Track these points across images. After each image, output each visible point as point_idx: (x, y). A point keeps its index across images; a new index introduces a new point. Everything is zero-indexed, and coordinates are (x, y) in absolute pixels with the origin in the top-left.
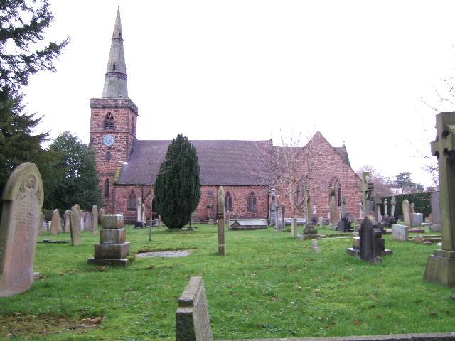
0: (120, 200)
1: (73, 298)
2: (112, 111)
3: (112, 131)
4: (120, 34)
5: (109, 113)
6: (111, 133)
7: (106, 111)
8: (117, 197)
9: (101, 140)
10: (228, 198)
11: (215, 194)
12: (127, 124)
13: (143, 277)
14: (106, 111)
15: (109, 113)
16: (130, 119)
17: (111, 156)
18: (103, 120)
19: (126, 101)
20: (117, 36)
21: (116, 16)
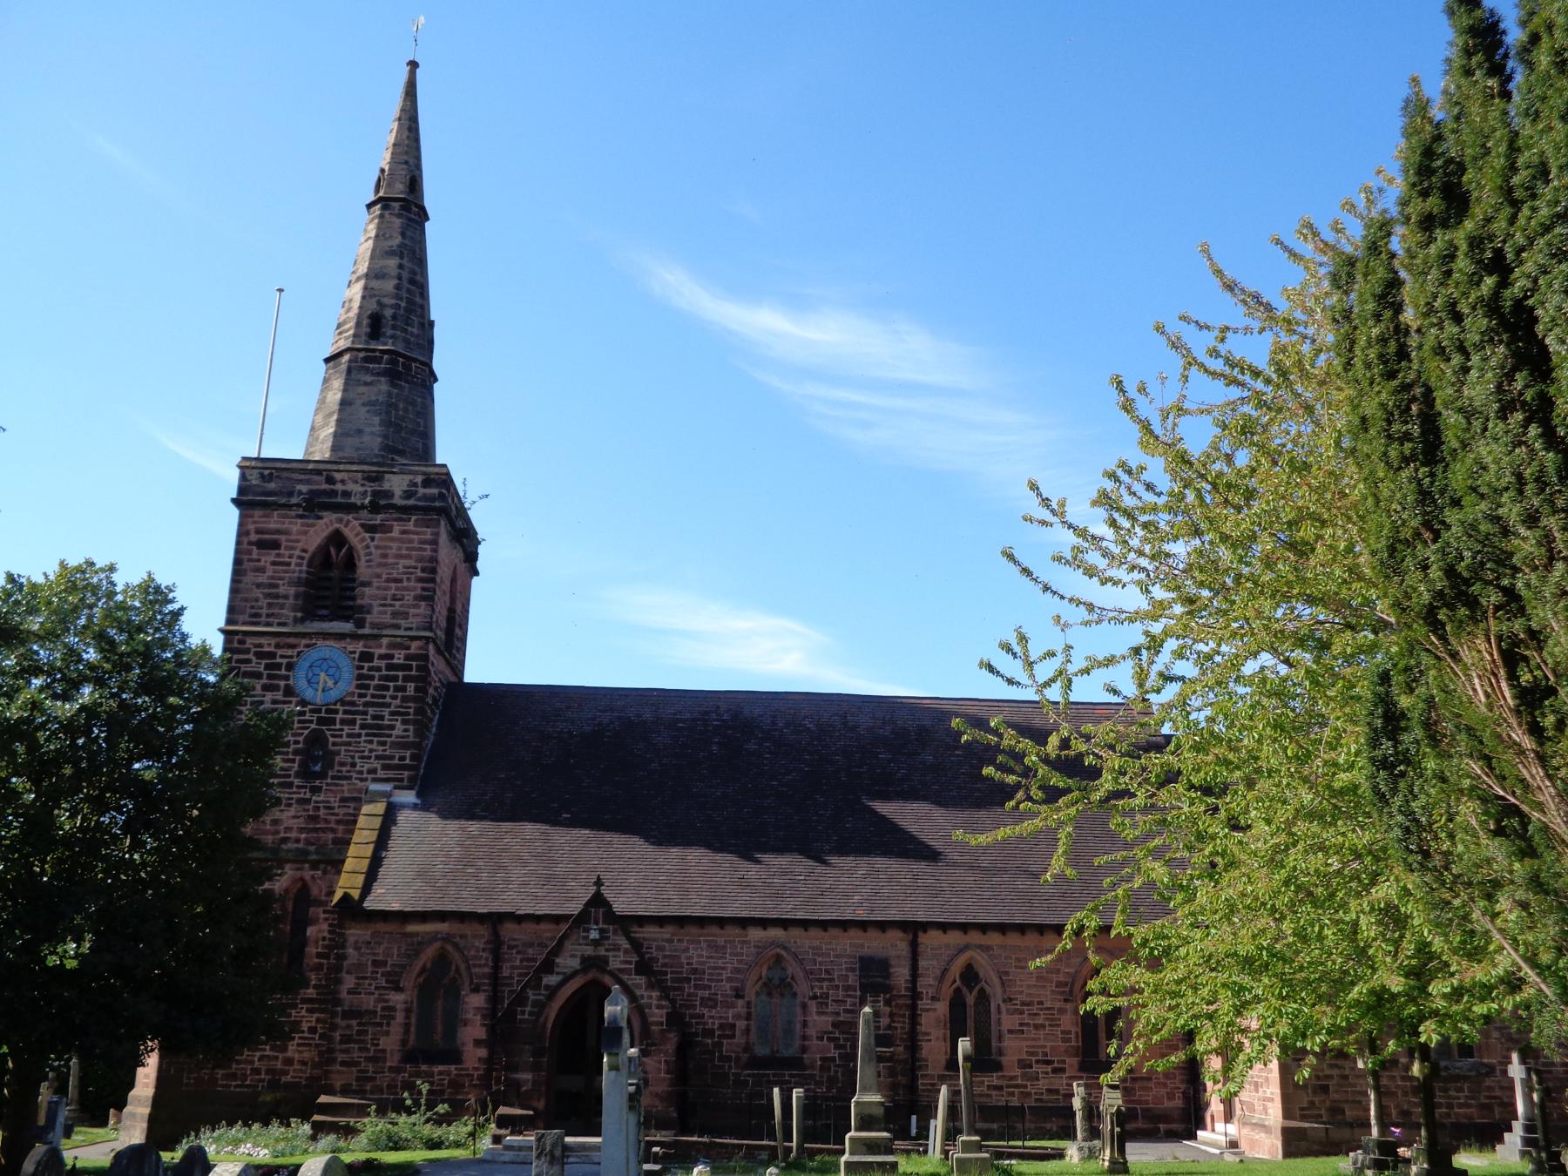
0: (369, 1002)
1: (1547, 229)
2: (352, 530)
3: (347, 627)
4: (415, 184)
5: (337, 539)
6: (341, 637)
7: (327, 523)
8: (349, 981)
9: (277, 672)
10: (970, 999)
11: (901, 974)
12: (427, 596)
13: (367, 429)
14: (315, 533)
15: (337, 539)
16: (444, 572)
17: (329, 759)
18: (298, 569)
19: (428, 482)
20: (399, 190)
21: (384, 159)
